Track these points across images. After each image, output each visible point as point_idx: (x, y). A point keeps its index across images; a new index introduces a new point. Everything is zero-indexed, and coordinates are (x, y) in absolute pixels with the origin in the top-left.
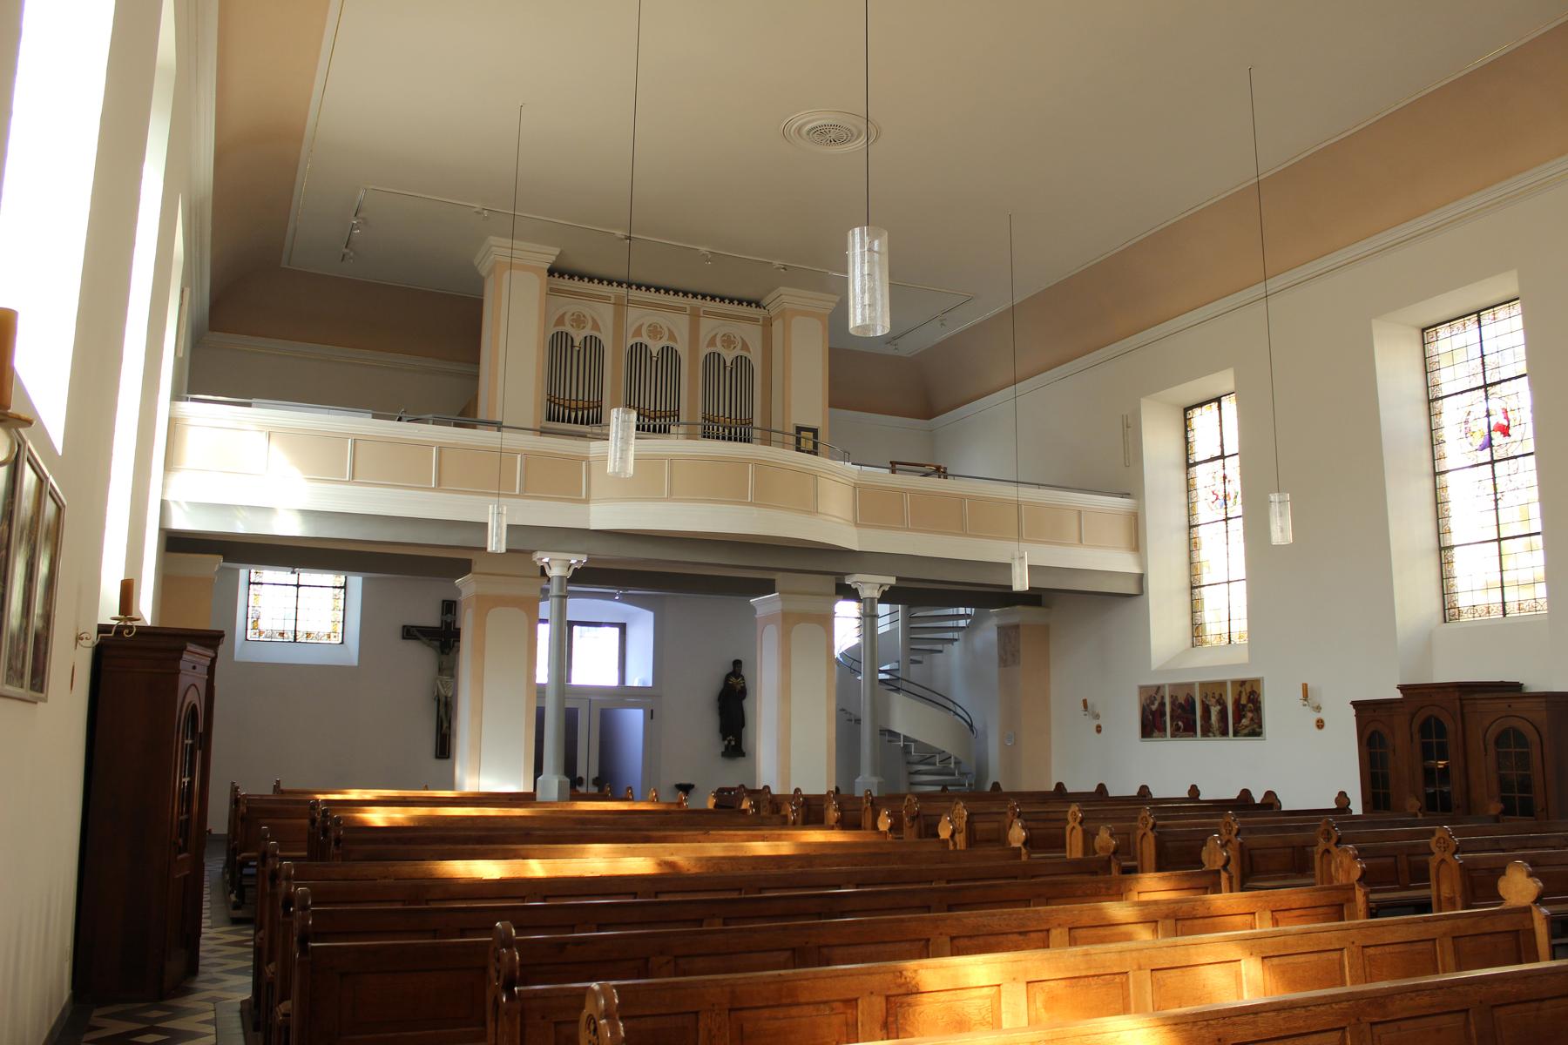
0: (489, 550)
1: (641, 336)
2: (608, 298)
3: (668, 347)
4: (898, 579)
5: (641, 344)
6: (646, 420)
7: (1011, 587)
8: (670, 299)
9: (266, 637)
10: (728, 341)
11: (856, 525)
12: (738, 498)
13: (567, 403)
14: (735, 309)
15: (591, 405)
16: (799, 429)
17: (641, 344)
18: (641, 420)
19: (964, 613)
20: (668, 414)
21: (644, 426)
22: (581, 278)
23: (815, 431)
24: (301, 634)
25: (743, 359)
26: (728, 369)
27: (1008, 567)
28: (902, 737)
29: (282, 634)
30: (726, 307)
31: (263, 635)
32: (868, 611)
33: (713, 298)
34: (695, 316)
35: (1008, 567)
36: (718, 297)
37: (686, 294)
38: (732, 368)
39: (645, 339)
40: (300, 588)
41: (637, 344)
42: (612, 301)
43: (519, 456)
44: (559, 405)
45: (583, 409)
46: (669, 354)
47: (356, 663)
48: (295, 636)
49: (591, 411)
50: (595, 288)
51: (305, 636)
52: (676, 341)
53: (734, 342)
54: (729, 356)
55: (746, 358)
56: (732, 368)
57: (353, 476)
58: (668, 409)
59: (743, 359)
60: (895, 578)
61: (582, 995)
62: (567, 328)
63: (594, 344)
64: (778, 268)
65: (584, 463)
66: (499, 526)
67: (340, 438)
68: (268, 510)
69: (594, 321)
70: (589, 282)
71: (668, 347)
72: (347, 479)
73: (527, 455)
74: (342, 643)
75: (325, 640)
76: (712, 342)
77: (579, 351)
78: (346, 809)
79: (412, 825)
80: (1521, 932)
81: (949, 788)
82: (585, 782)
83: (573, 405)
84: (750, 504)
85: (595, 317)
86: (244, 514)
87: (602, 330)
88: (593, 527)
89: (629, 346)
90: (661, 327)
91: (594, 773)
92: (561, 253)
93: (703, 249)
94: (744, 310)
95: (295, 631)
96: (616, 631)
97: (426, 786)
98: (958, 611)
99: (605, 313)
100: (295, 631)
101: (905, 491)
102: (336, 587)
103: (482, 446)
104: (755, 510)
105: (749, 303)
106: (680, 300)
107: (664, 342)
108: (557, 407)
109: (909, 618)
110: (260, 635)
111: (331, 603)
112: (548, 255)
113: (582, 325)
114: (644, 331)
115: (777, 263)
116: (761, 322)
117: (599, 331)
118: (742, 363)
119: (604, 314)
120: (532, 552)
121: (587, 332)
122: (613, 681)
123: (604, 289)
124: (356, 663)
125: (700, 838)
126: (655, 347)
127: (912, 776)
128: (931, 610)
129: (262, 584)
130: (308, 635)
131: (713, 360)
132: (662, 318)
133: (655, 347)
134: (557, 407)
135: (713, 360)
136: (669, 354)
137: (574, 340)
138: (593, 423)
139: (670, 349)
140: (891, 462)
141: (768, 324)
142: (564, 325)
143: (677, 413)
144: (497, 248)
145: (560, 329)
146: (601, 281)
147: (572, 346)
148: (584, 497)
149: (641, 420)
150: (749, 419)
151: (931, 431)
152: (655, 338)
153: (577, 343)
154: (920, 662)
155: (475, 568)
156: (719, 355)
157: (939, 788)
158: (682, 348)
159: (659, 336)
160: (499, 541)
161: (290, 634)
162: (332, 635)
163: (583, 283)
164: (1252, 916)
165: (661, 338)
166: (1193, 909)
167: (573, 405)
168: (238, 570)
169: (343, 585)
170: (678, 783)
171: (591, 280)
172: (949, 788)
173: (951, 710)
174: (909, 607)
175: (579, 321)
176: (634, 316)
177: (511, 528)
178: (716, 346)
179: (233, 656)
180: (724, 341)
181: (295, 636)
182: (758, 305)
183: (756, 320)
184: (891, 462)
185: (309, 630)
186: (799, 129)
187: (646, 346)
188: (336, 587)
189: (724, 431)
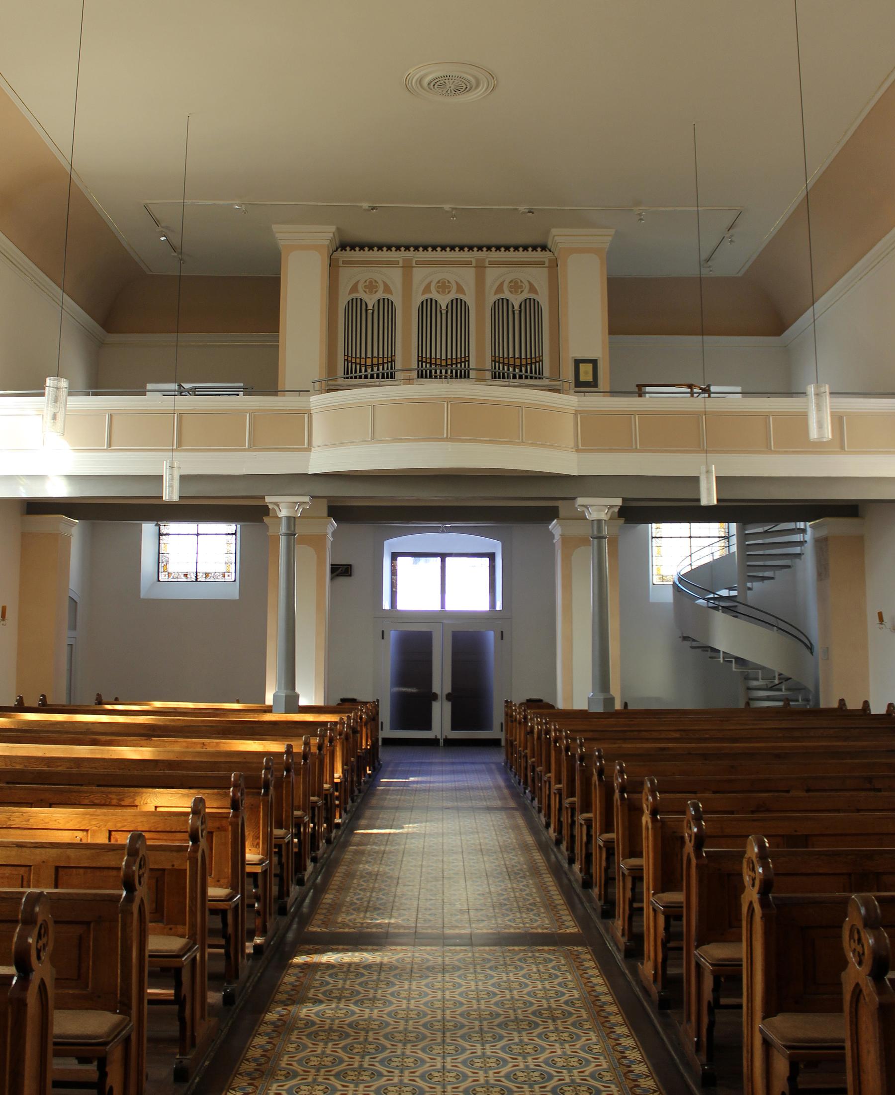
0: (164, 499)
1: (504, 293)
2: (397, 263)
3: (384, 299)
4: (624, 500)
5: (431, 300)
6: (428, 366)
7: (699, 500)
8: (457, 255)
9: (173, 578)
10: (516, 286)
11: (578, 450)
12: (433, 434)
13: (363, 361)
14: (521, 255)
15: (385, 360)
17: (431, 300)
18: (424, 366)
19: (794, 527)
20: (459, 360)
21: (383, 374)
22: (371, 248)
23: (594, 362)
24: (201, 574)
25: (532, 301)
26: (370, 312)
27: (696, 480)
28: (721, 653)
29: (186, 575)
30: (511, 255)
31: (171, 577)
32: (595, 532)
33: (498, 248)
34: (480, 267)
35: (694, 481)
36: (521, 246)
37: (471, 248)
38: (373, 311)
39: (434, 295)
40: (199, 536)
41: (427, 300)
42: (401, 265)
43: (248, 415)
44: (356, 363)
45: (531, 364)
46: (457, 306)
47: (237, 598)
48: (196, 576)
49: (533, 366)
50: (385, 255)
51: (204, 576)
52: (464, 293)
54: (516, 300)
55: (361, 300)
56: (373, 311)
57: (110, 445)
58: (459, 356)
59: (532, 301)
60: (621, 499)
62: (361, 295)
63: (386, 305)
64: (523, 213)
65: (306, 415)
66: (172, 479)
67: (99, 413)
68: (42, 478)
69: (386, 285)
70: (523, 251)
71: (384, 299)
72: (106, 448)
73: (254, 414)
74: (235, 581)
75: (221, 579)
76: (500, 289)
77: (373, 313)
78: (5, 715)
79: (13, 727)
80: (166, 872)
81: (791, 703)
82: (439, 697)
83: (518, 362)
84: (447, 439)
85: (389, 283)
86: (24, 480)
87: (466, 292)
88: (311, 471)
89: (419, 303)
90: (521, 281)
91: (448, 689)
92: (338, 229)
93: (447, 207)
94: (530, 255)
95: (196, 572)
96: (486, 561)
97: (116, 699)
98: (796, 525)
99: (394, 276)
100: (196, 572)
101: (631, 414)
102: (229, 534)
103: (260, 410)
104: (450, 445)
105: (534, 248)
106: (466, 255)
107: (453, 295)
108: (354, 366)
109: (743, 537)
110: (169, 577)
111: (225, 548)
112: (325, 234)
113: (374, 290)
114: (360, 287)
115: (522, 208)
116: (547, 265)
117: (464, 293)
118: (531, 307)
119: (394, 276)
120: (574, 499)
121: (380, 295)
122: (438, 607)
123: (393, 255)
124: (237, 598)
125: (142, 742)
126: (443, 301)
127: (750, 691)
128: (755, 528)
129: (168, 534)
130: (207, 575)
131: (501, 305)
132: (449, 274)
133: (443, 301)
134: (354, 366)
135: (501, 305)
136: (457, 306)
137: (368, 305)
138: (461, 376)
139: (459, 301)
140: (637, 386)
141: (554, 265)
142: (431, 292)
143: (467, 359)
144: (283, 234)
145: (354, 296)
146: (389, 248)
147: (366, 311)
148: (306, 445)
149: (424, 366)
150: (539, 357)
151: (785, 347)
152: (444, 292)
153: (370, 307)
154: (772, 578)
155: (562, 513)
156: (508, 300)
157: (781, 704)
158: (470, 299)
159: (447, 290)
160: (171, 492)
161: (192, 574)
162: (226, 574)
163: (455, 253)
165: (522, 292)
167: (518, 362)
168: (141, 524)
169: (234, 532)
170: (342, 698)
171: (380, 248)
172: (791, 703)
173: (774, 626)
174: (744, 524)
175: (371, 287)
176: (420, 275)
177: (183, 478)
178: (431, 292)
179: (139, 592)
180: (449, 287)
181: (196, 576)
182: (544, 248)
183: (543, 263)
184: (637, 386)
185: (208, 571)
187: (436, 301)
188: (229, 534)
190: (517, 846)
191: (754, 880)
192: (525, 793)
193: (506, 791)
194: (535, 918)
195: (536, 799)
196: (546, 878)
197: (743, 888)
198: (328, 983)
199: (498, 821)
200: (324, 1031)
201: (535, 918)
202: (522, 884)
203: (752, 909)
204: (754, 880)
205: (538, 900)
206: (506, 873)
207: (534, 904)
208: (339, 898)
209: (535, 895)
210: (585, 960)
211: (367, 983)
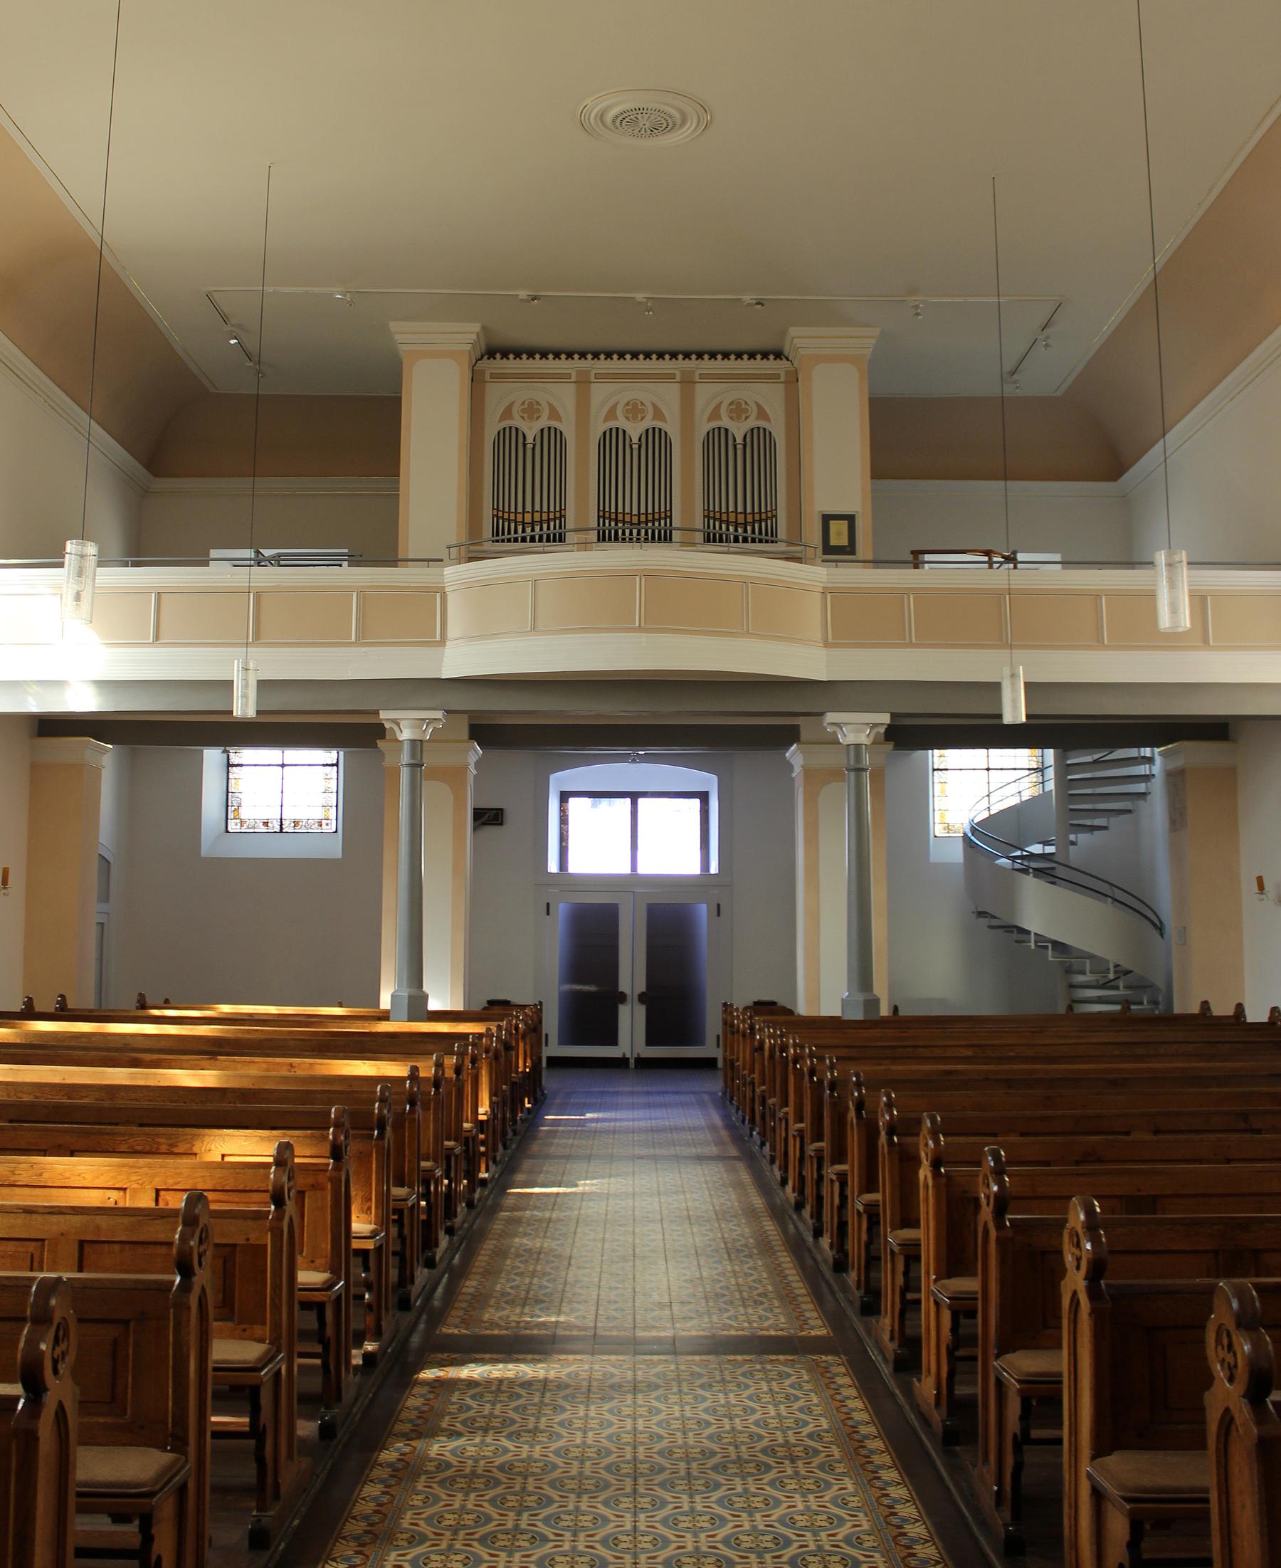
0: (235, 714)
1: (721, 419)
2: (568, 376)
3: (549, 428)
4: (893, 715)
5: (617, 429)
6: (613, 524)
7: (1000, 716)
8: (653, 365)
9: (248, 828)
10: (738, 410)
11: (827, 645)
12: (620, 622)
13: (519, 518)
14: (745, 365)
15: (552, 516)
16: (827, 519)
17: (617, 429)
18: (607, 525)
19: (1137, 755)
20: (657, 516)
22: (531, 355)
23: (850, 519)
24: (288, 822)
25: (761, 431)
26: (529, 447)
27: (996, 687)
28: (1033, 935)
29: (266, 824)
30: (732, 365)
31: (245, 826)
32: (852, 762)
33: (713, 355)
34: (688, 383)
35: (994, 689)
36: (746, 353)
37: (674, 355)
38: (534, 445)
39: (622, 423)
40: (285, 768)
41: (611, 429)
42: (573, 379)
43: (355, 594)
44: (509, 520)
45: (760, 521)
46: (654, 438)
47: (340, 856)
48: (281, 825)
49: (763, 524)
50: (551, 365)
51: (293, 825)
52: (664, 420)
53: (746, 411)
54: (738, 430)
55: (517, 429)
56: (534, 445)
57: (157, 637)
58: (657, 510)
59: (761, 431)
60: (889, 714)
61: (1210, 1291)
62: (517, 422)
63: (553, 437)
64: (749, 305)
65: (438, 595)
66: (246, 686)
67: (142, 592)
68: (59, 684)
69: (552, 408)
70: (749, 359)
71: (549, 428)
72: (151, 641)
73: (364, 593)
74: (336, 832)
75: (316, 829)
76: (715, 414)
77: (534, 449)
79: (18, 1041)
82: (629, 999)
83: (741, 519)
84: (640, 629)
85: (556, 405)
86: (34, 687)
87: (667, 418)
88: (445, 675)
89: (600, 433)
90: (746, 403)
92: (484, 328)
93: (640, 296)
94: (759, 365)
95: (281, 819)
96: (695, 803)
97: (167, 1001)
98: (1139, 752)
99: (564, 396)
100: (281, 819)
101: (903, 593)
102: (327, 765)
103: (372, 587)
104: (643, 637)
105: (765, 356)
106: (667, 365)
107: (648, 423)
108: (506, 524)
109: (1063, 769)
110: (241, 826)
111: (322, 785)
113: (536, 415)
114: (516, 411)
115: (748, 298)
116: (782, 379)
117: (664, 420)
118: (760, 439)
119: (564, 396)
120: (822, 714)
121: (544, 422)
122: (626, 870)
123: (563, 365)
124: (340, 856)
125: (203, 1063)
126: (635, 431)
127: (1073, 989)
128: (1080, 757)
129: (241, 765)
130: (296, 823)
131: (718, 437)
132: (643, 393)
133: (635, 431)
134: (506, 524)
135: (718, 437)
136: (654, 438)
137: (527, 437)
138: (660, 538)
139: (657, 431)
140: (912, 552)
141: (792, 380)
142: (617, 419)
143: (668, 514)
144: (405, 335)
145: (507, 423)
146: (557, 355)
147: (525, 445)
148: (438, 638)
149: (607, 525)
150: (771, 511)
151: (1124, 496)
153: (530, 440)
154: (1105, 828)
155: (804, 734)
156: (726, 430)
157: (1117, 1008)
158: (672, 428)
159: (639, 416)
160: (245, 704)
161: (275, 821)
162: (324, 822)
163: (651, 362)
164: (122, 1193)
165: (746, 418)
166: (13, 1173)
167: (741, 519)
168: (202, 751)
169: (335, 762)
170: (489, 999)
171: (544, 355)
172: (1133, 1007)
173: (1107, 896)
174: (1065, 751)
175: (531, 410)
176: (601, 394)
177: (262, 684)
178: (617, 419)
179: (200, 847)
180: (642, 411)
181: (281, 825)
182: (779, 355)
183: (777, 376)
184: (912, 552)
185: (297, 817)
186: (601, 116)
187: (624, 431)
188: (327, 765)
189: (736, 530)
190: (740, 1212)
191: (1079, 1259)
192: (751, 1135)
193: (724, 1133)
194: (766, 1314)
195: (768, 1145)
196: (782, 1257)
197: (1063, 1271)
198: (469, 1408)
199: (712, 1175)
200: (464, 1477)
201: (766, 1314)
202: (747, 1266)
203: (1076, 1301)
204: (1079, 1259)
205: (770, 1288)
206: (725, 1251)
207: (764, 1295)
208: (485, 1287)
209: (766, 1282)
210: (837, 1375)
211: (525, 1408)
